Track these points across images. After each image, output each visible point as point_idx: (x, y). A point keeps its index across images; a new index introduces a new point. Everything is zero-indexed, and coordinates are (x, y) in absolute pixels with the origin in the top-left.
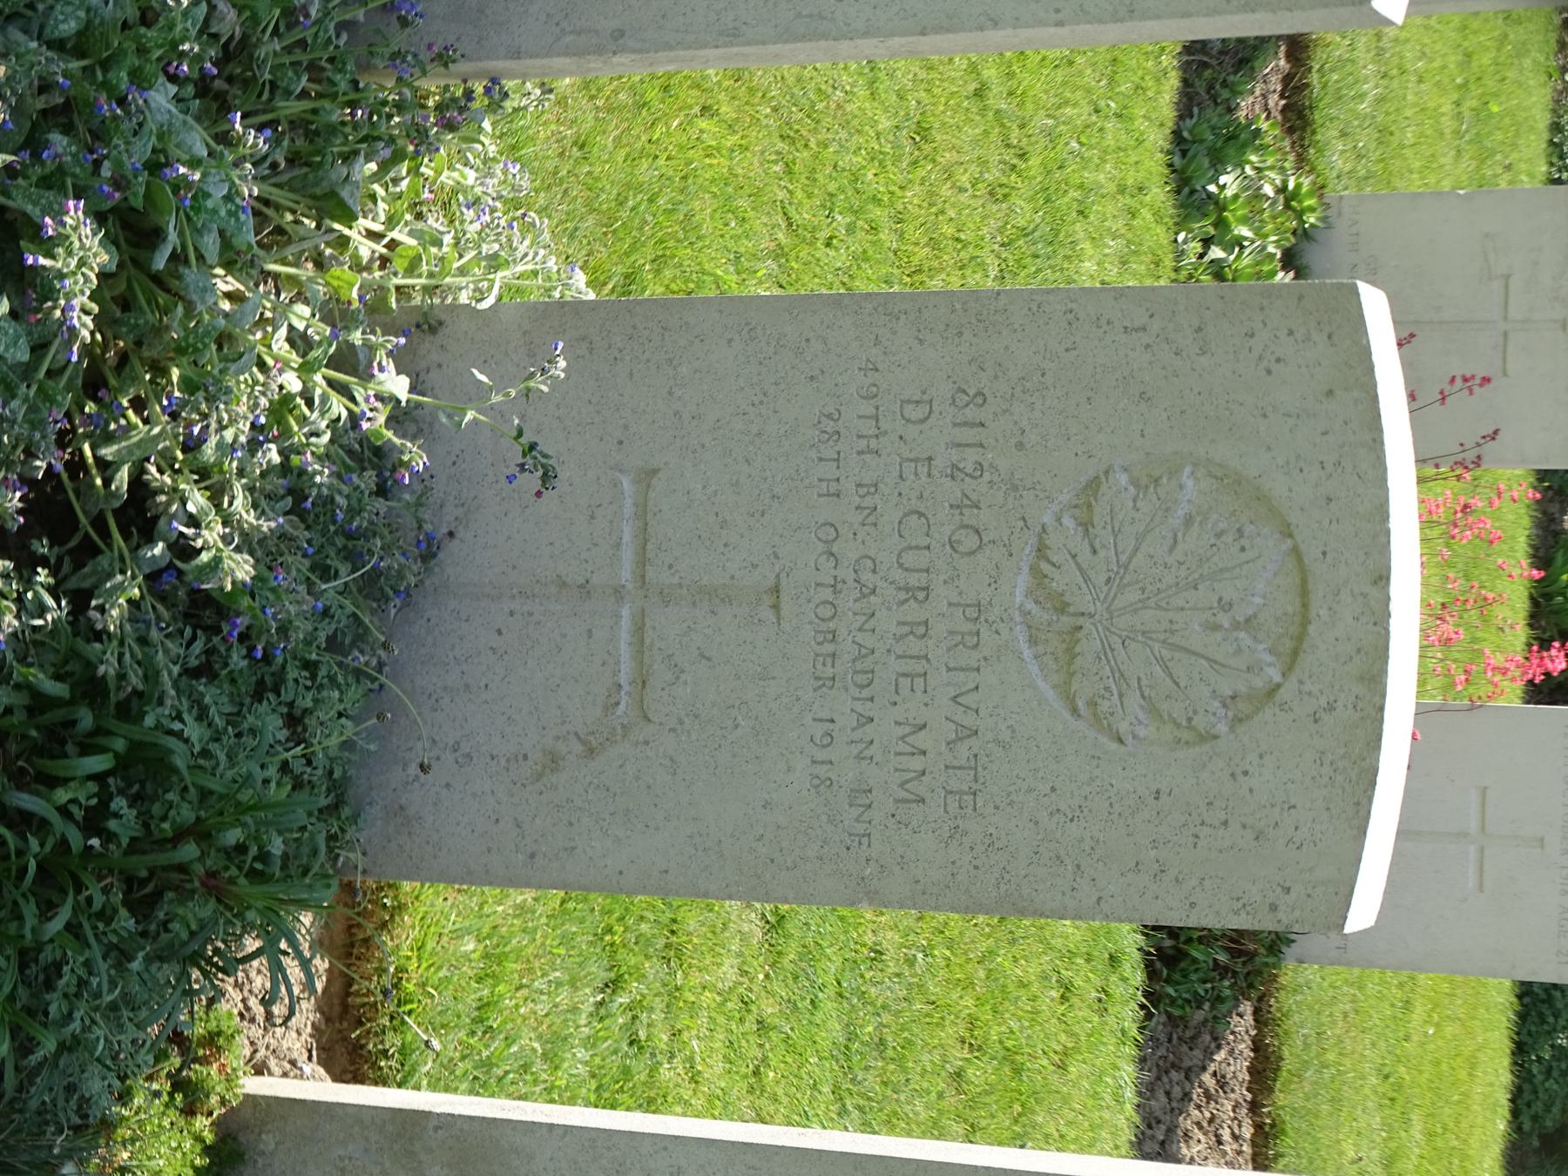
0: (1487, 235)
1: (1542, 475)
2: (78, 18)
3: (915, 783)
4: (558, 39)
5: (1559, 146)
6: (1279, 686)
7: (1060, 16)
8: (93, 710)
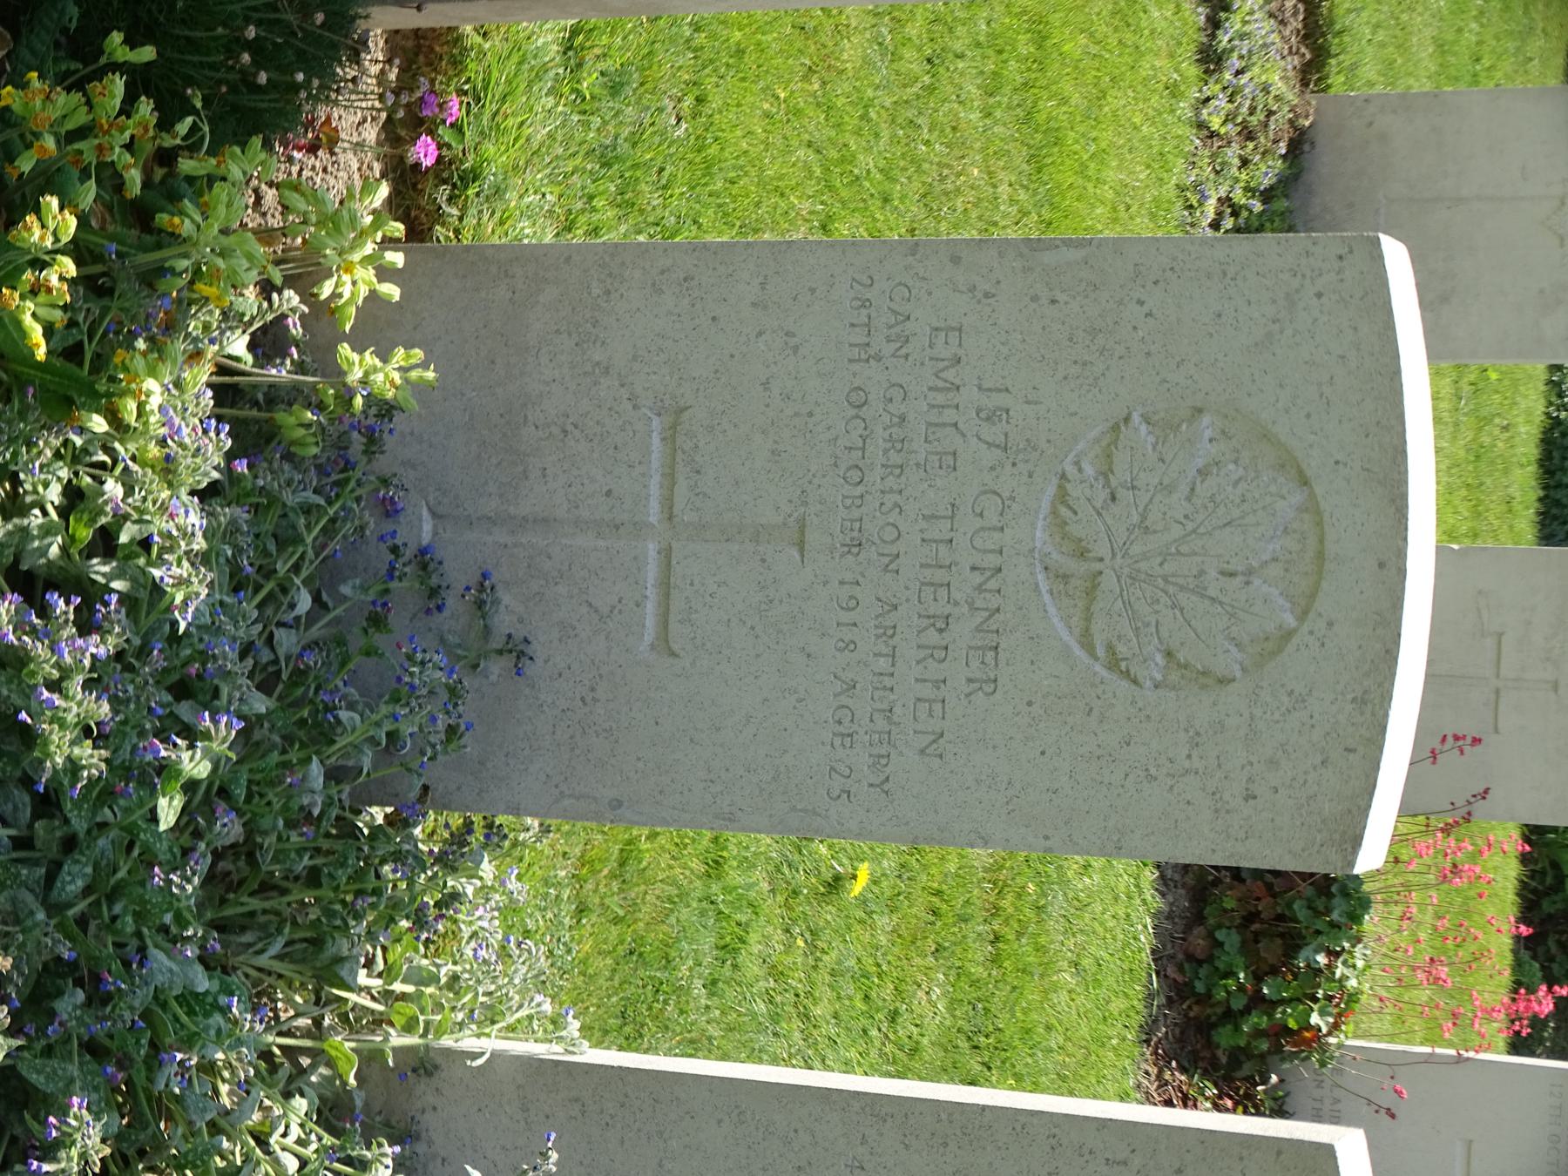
0: (1480, 592)
1: (1534, 834)
2: (85, 875)
3: (952, 371)
4: (557, 801)
5: (1558, 384)
6: (1288, 635)
7: (1048, 843)
8: (156, 379)
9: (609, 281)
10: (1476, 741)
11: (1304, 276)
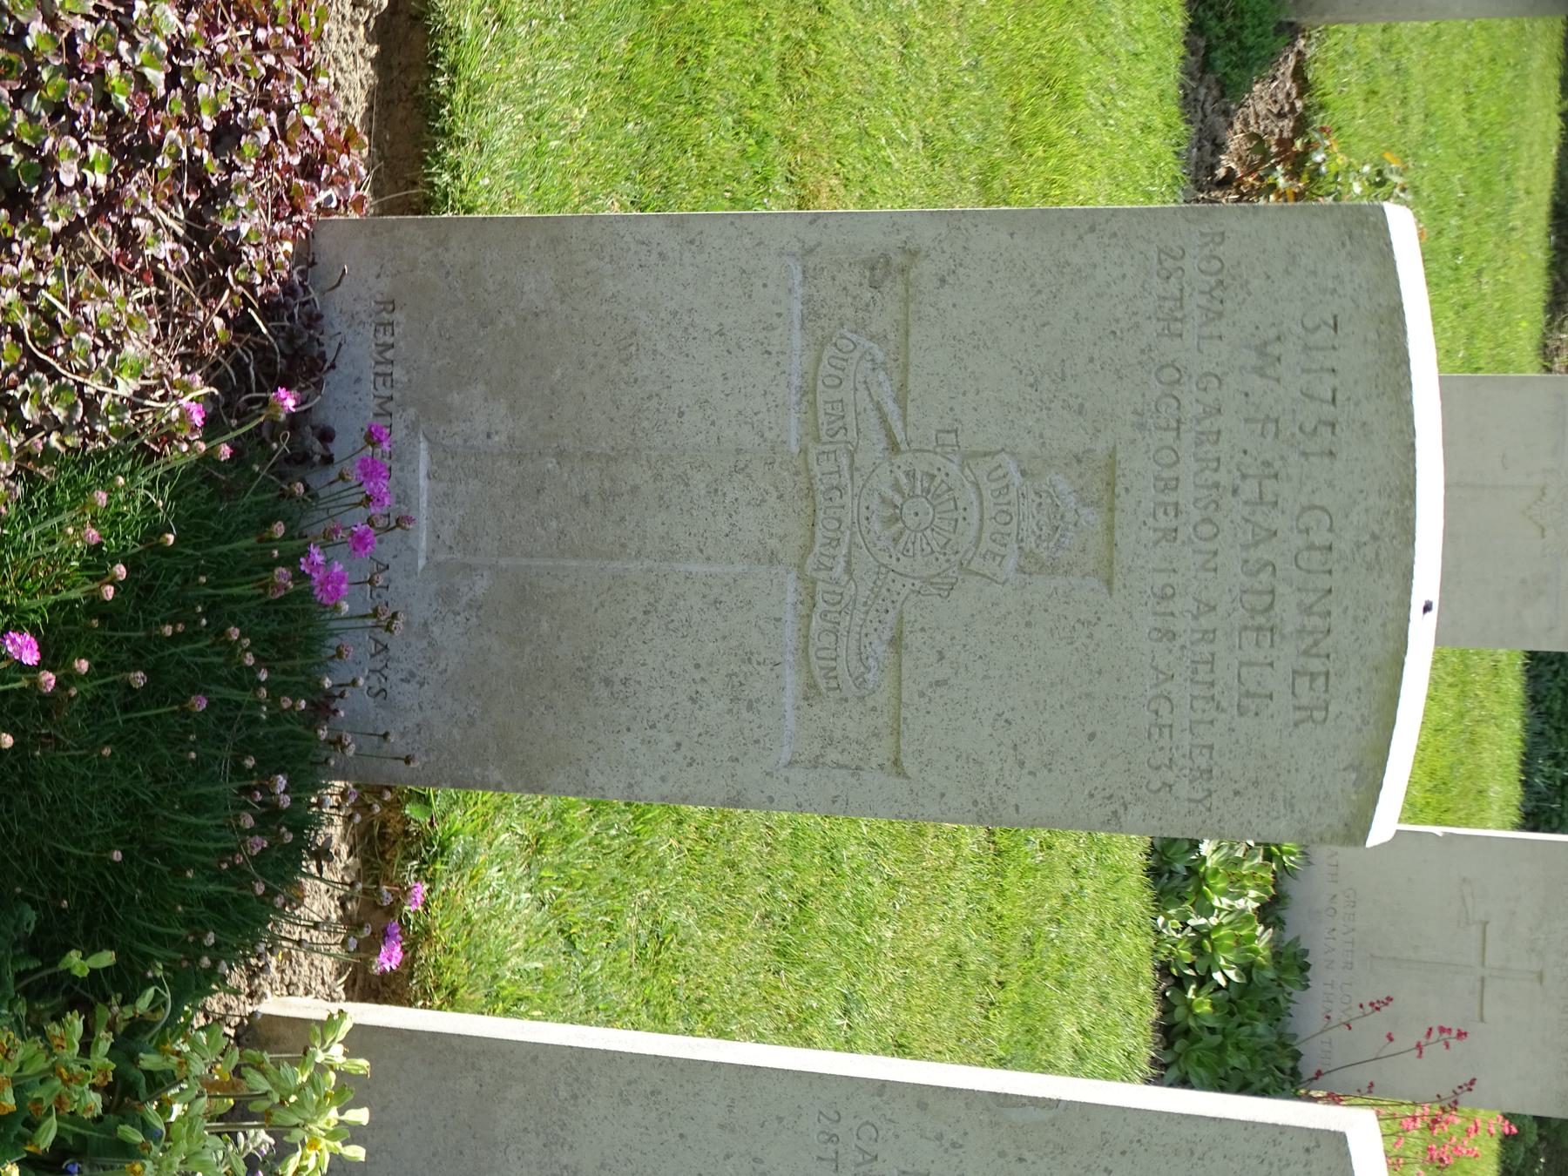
9: (576, 1086)
10: (1461, 1035)
11: (1271, 1164)
